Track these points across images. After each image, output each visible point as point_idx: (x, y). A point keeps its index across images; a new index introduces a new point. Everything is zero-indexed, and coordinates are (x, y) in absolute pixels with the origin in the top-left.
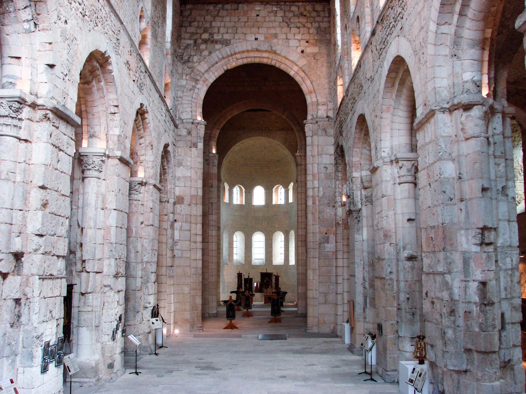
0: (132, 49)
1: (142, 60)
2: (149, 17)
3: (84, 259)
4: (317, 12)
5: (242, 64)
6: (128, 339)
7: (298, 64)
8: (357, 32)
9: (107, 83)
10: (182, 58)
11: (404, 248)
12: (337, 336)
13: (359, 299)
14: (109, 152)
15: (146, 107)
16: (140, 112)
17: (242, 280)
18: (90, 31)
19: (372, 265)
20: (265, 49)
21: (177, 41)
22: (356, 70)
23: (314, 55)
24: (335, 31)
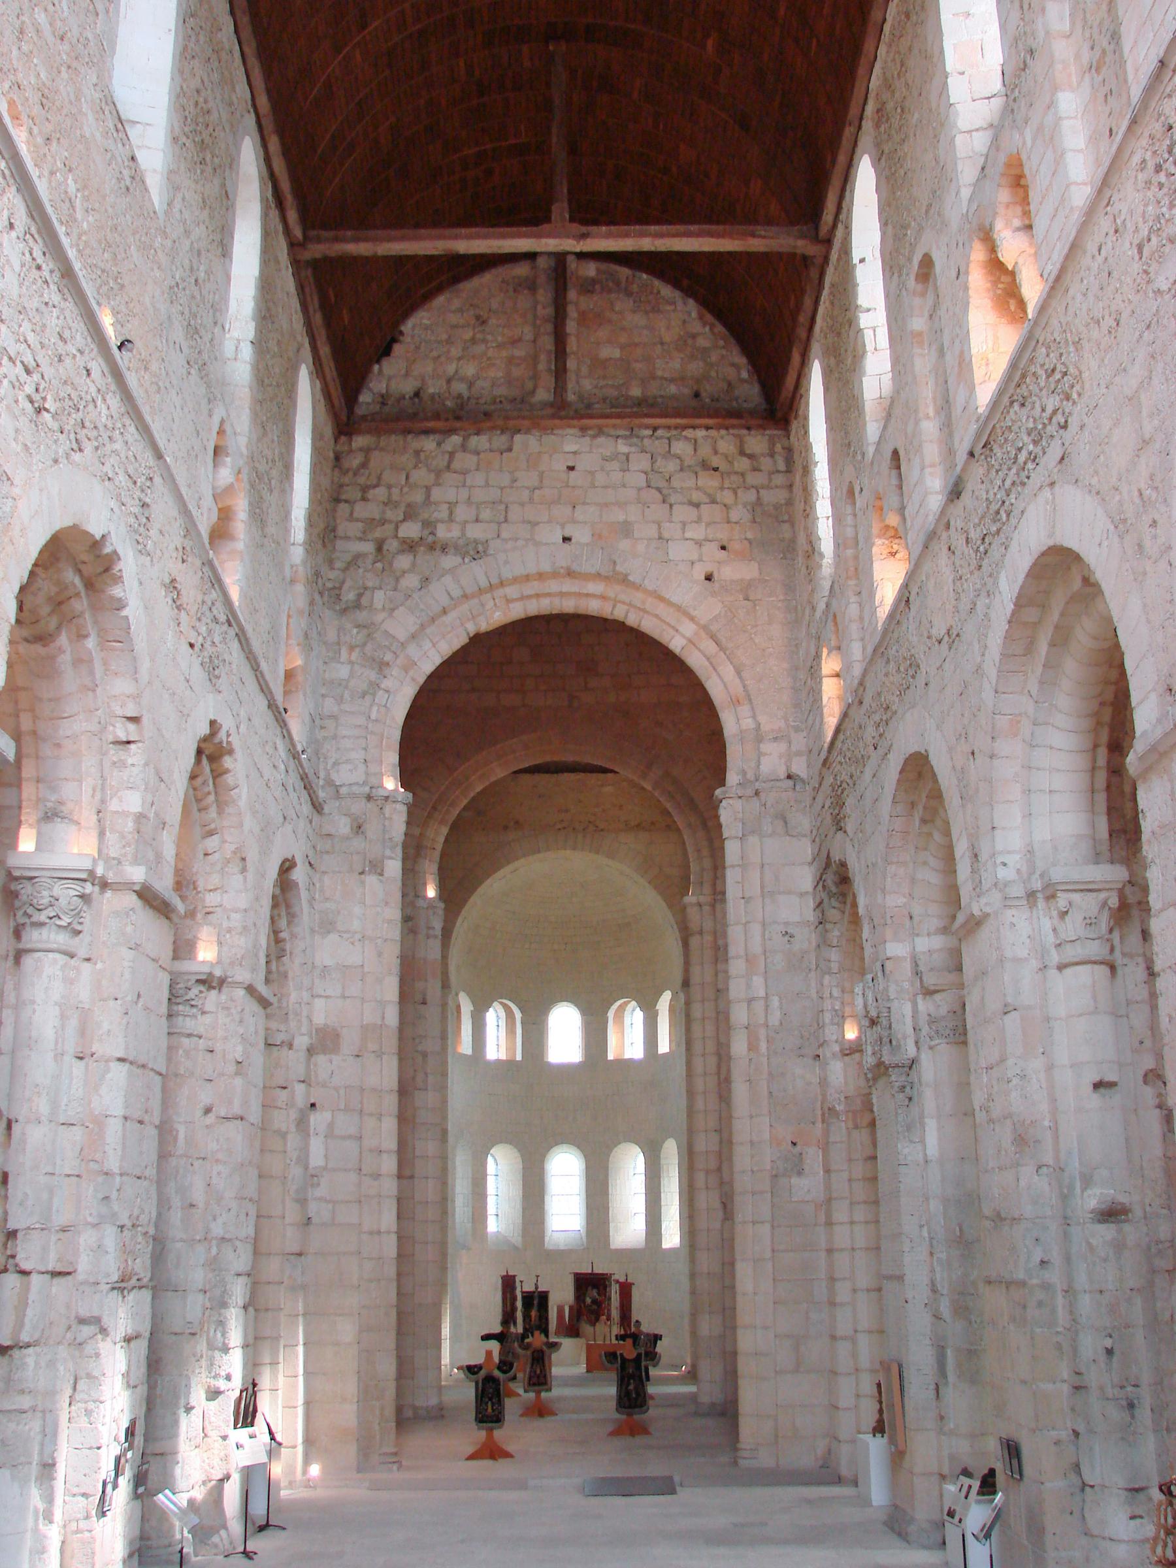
0: (188, 544)
1: (217, 582)
2: (241, 455)
3: (11, 1225)
4: (751, 457)
5: (523, 616)
6: (155, 1503)
7: (694, 613)
8: (893, 500)
9: (104, 641)
10: (338, 597)
11: (1087, 1181)
12: (839, 1480)
13: (920, 1359)
14: (108, 868)
15: (228, 735)
16: (209, 749)
17: (514, 1299)
18: (56, 461)
19: (964, 1243)
20: (593, 571)
21: (324, 546)
22: (891, 616)
23: (746, 589)
24: (808, 512)
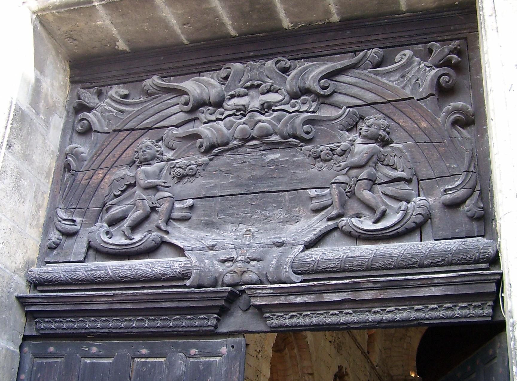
15: (346, 369)
